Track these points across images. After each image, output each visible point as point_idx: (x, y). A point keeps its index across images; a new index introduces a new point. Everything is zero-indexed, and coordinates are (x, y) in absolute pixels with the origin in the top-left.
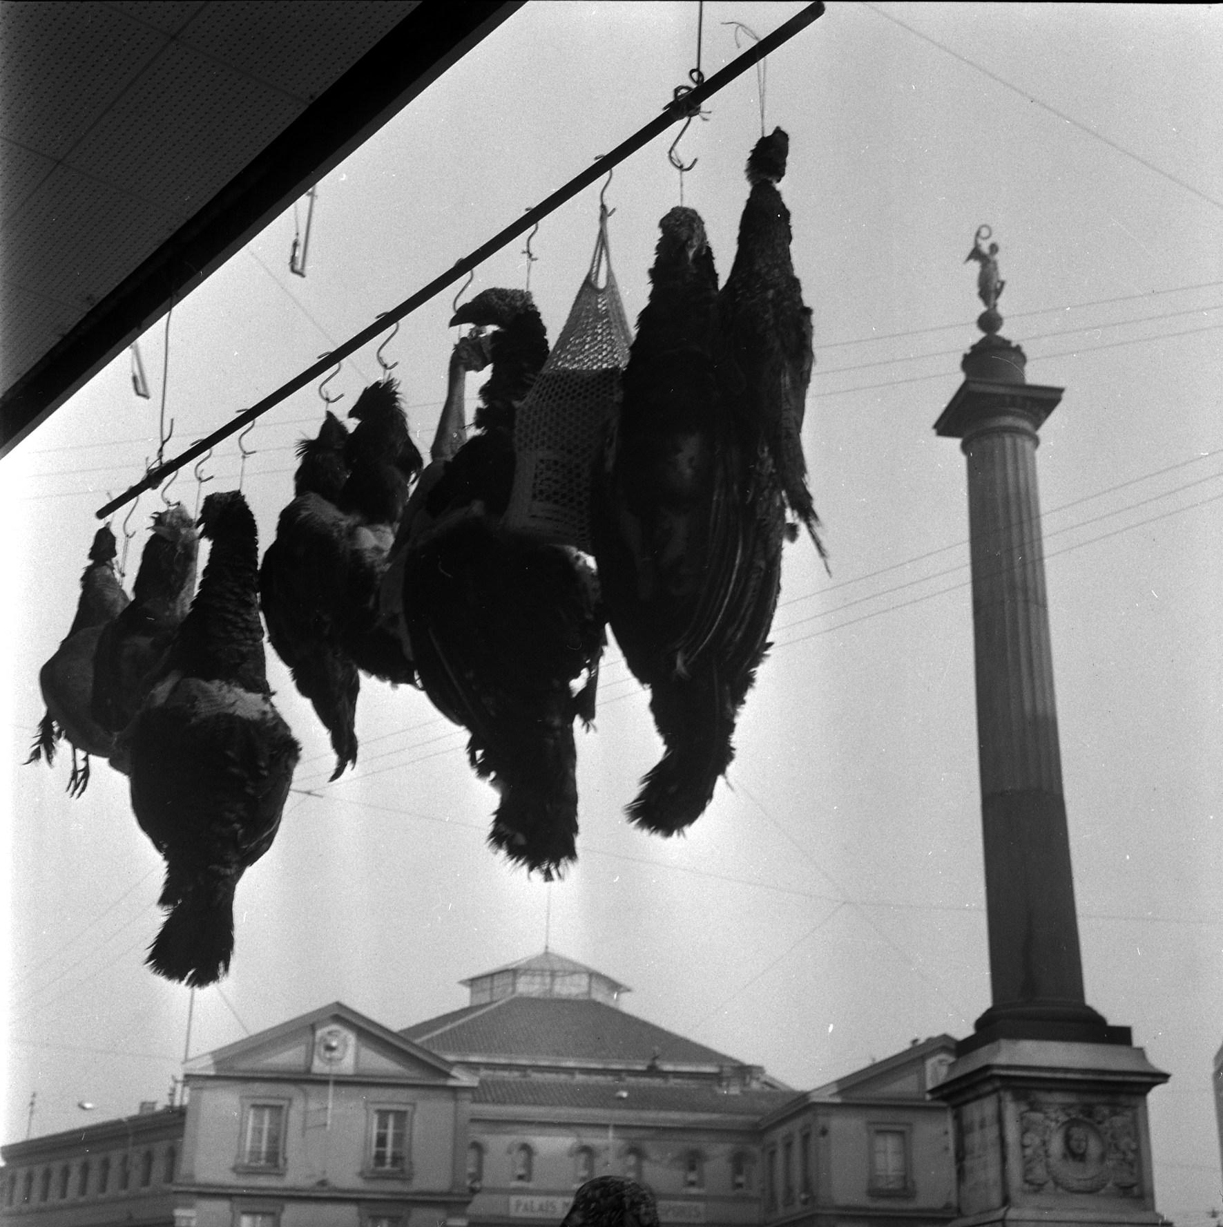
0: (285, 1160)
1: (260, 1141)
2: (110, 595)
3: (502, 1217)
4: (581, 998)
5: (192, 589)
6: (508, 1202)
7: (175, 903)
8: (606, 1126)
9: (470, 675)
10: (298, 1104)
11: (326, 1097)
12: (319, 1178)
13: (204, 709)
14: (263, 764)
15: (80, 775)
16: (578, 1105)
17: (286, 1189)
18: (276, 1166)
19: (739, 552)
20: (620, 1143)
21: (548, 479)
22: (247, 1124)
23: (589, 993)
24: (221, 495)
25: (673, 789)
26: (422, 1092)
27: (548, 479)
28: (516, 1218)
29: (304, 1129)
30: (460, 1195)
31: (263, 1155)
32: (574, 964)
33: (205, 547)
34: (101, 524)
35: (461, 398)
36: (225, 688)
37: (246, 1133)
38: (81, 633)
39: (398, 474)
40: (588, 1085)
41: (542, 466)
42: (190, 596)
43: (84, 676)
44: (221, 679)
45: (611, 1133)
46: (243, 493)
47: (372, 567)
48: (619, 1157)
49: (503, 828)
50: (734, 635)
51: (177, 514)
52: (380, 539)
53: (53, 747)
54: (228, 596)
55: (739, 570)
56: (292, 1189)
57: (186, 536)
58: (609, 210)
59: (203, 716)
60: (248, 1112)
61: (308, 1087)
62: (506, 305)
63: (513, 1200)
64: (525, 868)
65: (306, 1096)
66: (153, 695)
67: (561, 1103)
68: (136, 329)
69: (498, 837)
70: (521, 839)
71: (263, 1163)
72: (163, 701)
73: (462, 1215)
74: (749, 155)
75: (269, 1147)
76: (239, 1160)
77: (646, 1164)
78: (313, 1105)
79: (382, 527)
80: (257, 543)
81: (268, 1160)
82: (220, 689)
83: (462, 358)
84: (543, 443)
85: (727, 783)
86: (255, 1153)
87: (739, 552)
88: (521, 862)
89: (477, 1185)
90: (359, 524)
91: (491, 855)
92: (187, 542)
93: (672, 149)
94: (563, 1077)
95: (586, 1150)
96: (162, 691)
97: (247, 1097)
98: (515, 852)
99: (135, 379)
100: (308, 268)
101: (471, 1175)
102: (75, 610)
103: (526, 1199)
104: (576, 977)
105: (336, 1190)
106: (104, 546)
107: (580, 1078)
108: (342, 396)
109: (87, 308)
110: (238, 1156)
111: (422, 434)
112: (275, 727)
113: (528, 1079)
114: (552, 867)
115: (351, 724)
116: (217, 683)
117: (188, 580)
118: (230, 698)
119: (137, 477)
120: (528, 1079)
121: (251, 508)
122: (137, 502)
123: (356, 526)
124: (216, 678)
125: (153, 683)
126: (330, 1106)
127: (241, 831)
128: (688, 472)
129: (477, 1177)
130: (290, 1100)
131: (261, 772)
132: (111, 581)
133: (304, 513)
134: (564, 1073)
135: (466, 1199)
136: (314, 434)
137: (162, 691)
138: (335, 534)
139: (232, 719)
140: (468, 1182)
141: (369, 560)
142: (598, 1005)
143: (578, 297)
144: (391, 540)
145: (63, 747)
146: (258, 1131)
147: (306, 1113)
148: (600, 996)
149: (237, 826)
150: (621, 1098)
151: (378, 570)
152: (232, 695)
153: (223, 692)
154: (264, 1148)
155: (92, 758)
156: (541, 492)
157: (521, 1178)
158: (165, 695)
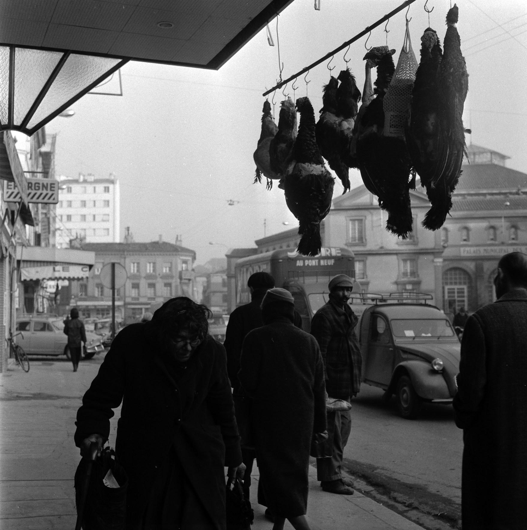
0: (366, 240)
1: (355, 233)
2: (271, 126)
3: (458, 256)
4: (487, 163)
5: (296, 128)
6: (460, 251)
7: (303, 234)
8: (501, 217)
9: (377, 181)
10: (369, 218)
11: (380, 215)
12: (380, 245)
13: (304, 173)
14: (323, 190)
15: (270, 183)
16: (488, 210)
17: (367, 251)
18: (363, 242)
19: (448, 150)
20: (508, 224)
21: (394, 121)
22: (349, 227)
23: (491, 160)
24: (301, 99)
25: (434, 218)
26: (420, 209)
27: (394, 121)
28: (464, 257)
29: (373, 227)
30: (438, 249)
31: (357, 238)
32: (483, 149)
33: (298, 115)
34: (264, 99)
35: (370, 79)
36: (310, 165)
37: (349, 230)
38: (264, 141)
39: (353, 101)
40: (492, 200)
41: (392, 117)
42: (296, 130)
43: (267, 157)
44: (308, 162)
45: (503, 220)
46: (308, 97)
47: (347, 135)
48: (507, 229)
49: (390, 225)
50: (448, 174)
51: (288, 102)
52: (349, 124)
53: (260, 177)
54: (307, 135)
55: (448, 155)
56: (370, 251)
57: (292, 110)
58: (409, 20)
59: (304, 176)
60: (349, 223)
61: (372, 211)
62: (380, 53)
63: (462, 249)
64: (397, 235)
65: (372, 214)
66: (288, 171)
67: (481, 209)
68: (266, 22)
69: (388, 228)
70: (395, 228)
71: (357, 241)
72: (292, 172)
73: (441, 257)
74: (446, 19)
75: (359, 236)
76: (348, 241)
77: (519, 232)
78: (375, 218)
79: (350, 120)
80: (314, 114)
81: (359, 240)
82: (308, 166)
83: (369, 65)
84: (392, 110)
85: (450, 215)
86: (354, 238)
87: (448, 150)
88: (396, 234)
89: (446, 245)
90: (343, 120)
91: (387, 232)
92: (293, 112)
93: (425, 5)
94: (481, 197)
95: (493, 228)
96: (291, 168)
97: (348, 217)
98: (394, 231)
99: (268, 39)
100: (321, 8)
101: (443, 240)
102: (261, 130)
103: (468, 249)
104: (485, 154)
105: (387, 250)
106: (267, 107)
107: (488, 197)
108: (335, 67)
109: (250, 20)
110: (347, 240)
111: (360, 85)
112: (326, 176)
113: (466, 200)
114: (405, 235)
115: (348, 177)
116: (307, 164)
117: (294, 125)
118: (312, 168)
119: (275, 85)
120: (466, 200)
121: (312, 104)
122: (275, 92)
123: (341, 122)
124: (306, 162)
125: (287, 167)
126: (382, 217)
127: (319, 211)
128: (431, 127)
129: (446, 241)
130: (365, 217)
131: (323, 192)
132: (271, 122)
133: (325, 120)
134: (481, 195)
135: (441, 251)
136: (327, 83)
137: (291, 168)
138: (335, 126)
139: (313, 176)
140: (442, 243)
141: (346, 133)
142: (496, 166)
143: (400, 56)
144: (353, 123)
145: (264, 178)
146: (354, 229)
147: (372, 221)
148: (496, 161)
149: (318, 209)
150: (507, 205)
151: (349, 136)
152: (312, 167)
153: (309, 167)
154: (357, 235)
155: (273, 180)
156: (392, 125)
157: (465, 240)
158: (292, 170)
